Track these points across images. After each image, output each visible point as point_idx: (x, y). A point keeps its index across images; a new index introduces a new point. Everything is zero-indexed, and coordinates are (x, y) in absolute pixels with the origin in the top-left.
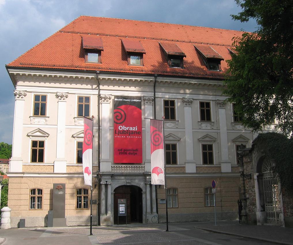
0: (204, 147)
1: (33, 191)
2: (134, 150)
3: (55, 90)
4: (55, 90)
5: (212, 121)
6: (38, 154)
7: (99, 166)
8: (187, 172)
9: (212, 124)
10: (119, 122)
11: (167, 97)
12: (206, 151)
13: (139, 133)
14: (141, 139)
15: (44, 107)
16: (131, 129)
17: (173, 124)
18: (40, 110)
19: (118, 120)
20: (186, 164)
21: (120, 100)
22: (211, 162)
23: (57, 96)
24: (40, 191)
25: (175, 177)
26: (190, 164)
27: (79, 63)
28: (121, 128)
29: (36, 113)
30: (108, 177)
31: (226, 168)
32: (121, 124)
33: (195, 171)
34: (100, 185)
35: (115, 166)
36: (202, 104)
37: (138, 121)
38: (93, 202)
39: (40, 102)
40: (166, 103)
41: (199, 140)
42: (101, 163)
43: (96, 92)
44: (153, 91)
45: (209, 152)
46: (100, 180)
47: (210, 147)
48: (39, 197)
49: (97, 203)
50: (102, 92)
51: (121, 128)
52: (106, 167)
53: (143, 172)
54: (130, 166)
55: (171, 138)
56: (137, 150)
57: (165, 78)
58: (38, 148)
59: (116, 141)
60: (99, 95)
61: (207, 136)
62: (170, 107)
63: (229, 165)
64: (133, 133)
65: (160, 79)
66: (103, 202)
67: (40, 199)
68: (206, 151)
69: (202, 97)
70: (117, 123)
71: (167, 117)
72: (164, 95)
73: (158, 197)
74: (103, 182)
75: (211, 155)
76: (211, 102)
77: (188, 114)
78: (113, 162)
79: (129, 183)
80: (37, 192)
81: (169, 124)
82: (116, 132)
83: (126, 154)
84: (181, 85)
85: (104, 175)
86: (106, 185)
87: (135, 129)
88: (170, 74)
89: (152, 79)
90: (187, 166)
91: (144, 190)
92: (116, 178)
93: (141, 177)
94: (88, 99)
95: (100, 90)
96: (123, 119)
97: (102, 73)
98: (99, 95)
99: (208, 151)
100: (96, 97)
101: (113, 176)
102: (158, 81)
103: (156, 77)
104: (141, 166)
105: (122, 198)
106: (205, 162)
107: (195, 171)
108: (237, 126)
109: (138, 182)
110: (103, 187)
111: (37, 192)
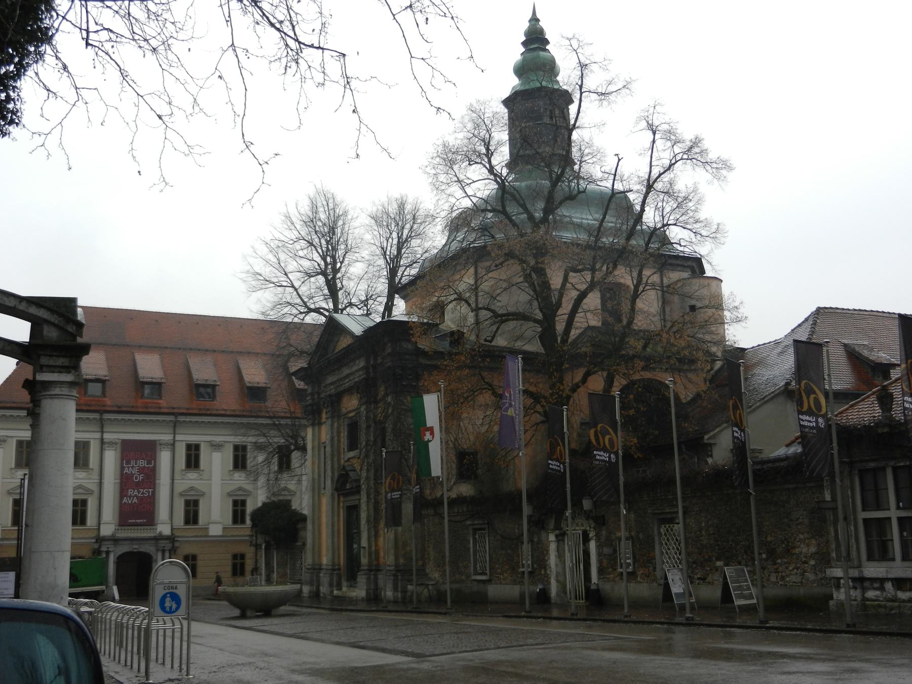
0: (235, 503)
1: (235, 557)
3: (209, 438)
4: (209, 438)
5: (91, 466)
6: (192, 516)
7: (99, 529)
11: (193, 439)
18: (193, 460)
22: (196, 522)
25: (193, 541)
30: (110, 542)
36: (236, 448)
39: (240, 454)
40: (189, 447)
41: (229, 495)
42: (102, 526)
43: (98, 435)
44: (99, 429)
47: (196, 503)
50: (106, 436)
60: (102, 439)
62: (193, 452)
65: (181, 418)
69: (238, 440)
77: (217, 463)
81: (192, 475)
89: (172, 418)
91: (154, 557)
93: (153, 542)
95: (102, 432)
98: (102, 439)
99: (239, 508)
100: (98, 443)
101: (115, 540)
103: (101, 414)
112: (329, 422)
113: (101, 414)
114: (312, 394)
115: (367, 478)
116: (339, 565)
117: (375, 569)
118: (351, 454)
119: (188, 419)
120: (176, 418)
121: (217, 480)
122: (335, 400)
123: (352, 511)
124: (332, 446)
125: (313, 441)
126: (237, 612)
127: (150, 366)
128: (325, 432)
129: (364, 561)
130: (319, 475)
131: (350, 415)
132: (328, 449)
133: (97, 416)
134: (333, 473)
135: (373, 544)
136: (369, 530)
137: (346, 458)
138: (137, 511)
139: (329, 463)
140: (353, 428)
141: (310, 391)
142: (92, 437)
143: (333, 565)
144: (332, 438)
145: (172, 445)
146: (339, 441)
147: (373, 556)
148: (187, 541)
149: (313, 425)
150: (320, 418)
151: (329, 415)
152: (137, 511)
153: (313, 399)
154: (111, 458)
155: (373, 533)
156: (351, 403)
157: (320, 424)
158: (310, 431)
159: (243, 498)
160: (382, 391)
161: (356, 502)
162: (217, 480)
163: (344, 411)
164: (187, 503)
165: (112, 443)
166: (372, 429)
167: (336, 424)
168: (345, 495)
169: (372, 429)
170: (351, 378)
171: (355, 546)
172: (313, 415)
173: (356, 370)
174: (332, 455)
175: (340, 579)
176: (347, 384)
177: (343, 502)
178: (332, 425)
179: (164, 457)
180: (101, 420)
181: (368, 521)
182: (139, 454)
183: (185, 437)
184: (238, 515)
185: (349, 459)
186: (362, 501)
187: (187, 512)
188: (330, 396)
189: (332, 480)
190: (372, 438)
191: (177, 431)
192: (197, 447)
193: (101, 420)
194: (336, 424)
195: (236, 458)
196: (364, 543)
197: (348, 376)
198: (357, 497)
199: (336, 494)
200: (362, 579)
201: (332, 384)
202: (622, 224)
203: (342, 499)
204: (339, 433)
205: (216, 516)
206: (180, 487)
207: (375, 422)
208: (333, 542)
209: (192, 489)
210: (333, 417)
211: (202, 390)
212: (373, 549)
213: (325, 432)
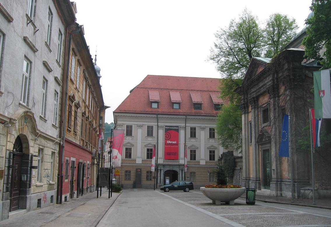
0: (210, 152)
1: (126, 171)
2: (174, 153)
6: (193, 156)
8: (200, 164)
9: (133, 137)
10: (167, 139)
11: (193, 125)
12: (213, 154)
13: (177, 144)
14: (178, 147)
15: (131, 131)
16: (173, 142)
17: (151, 139)
18: (193, 134)
19: (167, 138)
20: (201, 160)
21: (168, 128)
22: (195, 159)
23: (138, 126)
24: (130, 172)
25: (195, 167)
26: (139, 159)
27: (148, 109)
28: (168, 142)
29: (210, 137)
31: (203, 163)
32: (168, 140)
33: (141, 163)
34: (158, 170)
35: (165, 160)
36: (210, 129)
37: (177, 139)
38: (154, 178)
39: (193, 131)
40: (191, 129)
41: (208, 148)
43: (156, 124)
44: (157, 122)
45: (194, 154)
46: (158, 168)
47: (195, 151)
48: (129, 175)
49: (156, 178)
51: (168, 142)
52: (161, 161)
53: (179, 164)
54: (172, 161)
55: (193, 147)
56: (176, 153)
57: (191, 116)
58: (212, 154)
59: (166, 149)
60: (158, 125)
61: (212, 146)
62: (193, 131)
63: (141, 160)
64: (174, 144)
65: (188, 117)
66: (159, 178)
67: (130, 175)
68: (213, 154)
70: (166, 140)
71: (191, 136)
72: (190, 125)
73: (186, 176)
74: (159, 168)
75: (214, 156)
76: (197, 127)
77: (203, 135)
78: (164, 158)
79: (171, 169)
80: (149, 173)
81: (193, 140)
82: (166, 144)
83: (170, 155)
84: (163, 118)
85: (159, 165)
86: (161, 170)
87: (175, 142)
88: (194, 114)
89: (185, 117)
90: (201, 161)
92: (166, 166)
93: (178, 166)
94: (152, 127)
96: (169, 138)
97: (189, 115)
98: (158, 125)
99: (212, 154)
101: (164, 166)
102: (187, 118)
104: (177, 161)
105: (168, 176)
106: (210, 159)
107: (141, 163)
108: (191, 140)
109: (176, 169)
110: (159, 171)
111: (149, 173)
112: (253, 110)
113: (157, 115)
114: (244, 99)
115: (275, 135)
116: (259, 178)
117: (280, 181)
118: (265, 124)
119: (191, 117)
120: (186, 116)
121: (203, 143)
122: (256, 100)
123: (266, 153)
124: (255, 122)
125: (245, 120)
126: (211, 201)
127: (176, 97)
128: (251, 116)
129: (274, 176)
130: (248, 137)
131: (264, 106)
132: (253, 123)
133: (155, 116)
134: (255, 134)
135: (279, 168)
136: (276, 161)
137: (262, 127)
138: (171, 153)
139: (253, 129)
140: (266, 112)
141: (243, 98)
142: (154, 124)
143: (256, 178)
144: (255, 118)
145: (185, 128)
146: (258, 119)
147: (279, 174)
148: (192, 167)
149: (245, 113)
150: (248, 110)
151: (253, 107)
152: (171, 153)
153: (244, 101)
154: (161, 133)
155: (279, 163)
156: (264, 100)
157: (248, 113)
158: (243, 116)
159: (214, 150)
160: (282, 90)
161: (269, 148)
162: (203, 143)
163: (260, 104)
164: (191, 151)
165: (162, 127)
166: (277, 110)
167: (256, 112)
168: (262, 145)
169: (277, 110)
170: (264, 87)
171: (268, 169)
172: (245, 108)
173: (268, 81)
174: (255, 126)
175: (260, 185)
176: (262, 90)
177: (261, 148)
178: (255, 112)
179: (182, 133)
180: (157, 117)
181: (276, 157)
182: (171, 133)
183: (190, 125)
184: (212, 156)
185: (264, 127)
186: (272, 147)
187: (191, 133)
188: (254, 98)
189: (255, 138)
190: (277, 115)
191: (187, 122)
192: (195, 129)
193: (157, 117)
194: (256, 112)
195: (210, 134)
196: (274, 167)
197: (262, 86)
198: (269, 145)
199: (257, 145)
200: (273, 185)
201: (253, 92)
202: (302, 109)
203: (260, 147)
204: (258, 115)
205: (203, 157)
206: (189, 144)
207: (278, 107)
208: (256, 168)
209: (193, 146)
210: (255, 108)
211: (196, 106)
212: (279, 170)
213: (251, 116)
